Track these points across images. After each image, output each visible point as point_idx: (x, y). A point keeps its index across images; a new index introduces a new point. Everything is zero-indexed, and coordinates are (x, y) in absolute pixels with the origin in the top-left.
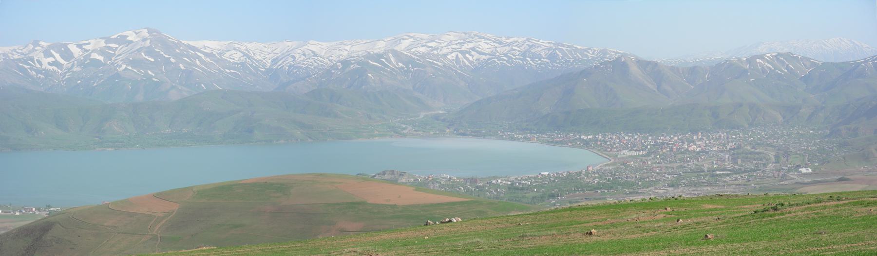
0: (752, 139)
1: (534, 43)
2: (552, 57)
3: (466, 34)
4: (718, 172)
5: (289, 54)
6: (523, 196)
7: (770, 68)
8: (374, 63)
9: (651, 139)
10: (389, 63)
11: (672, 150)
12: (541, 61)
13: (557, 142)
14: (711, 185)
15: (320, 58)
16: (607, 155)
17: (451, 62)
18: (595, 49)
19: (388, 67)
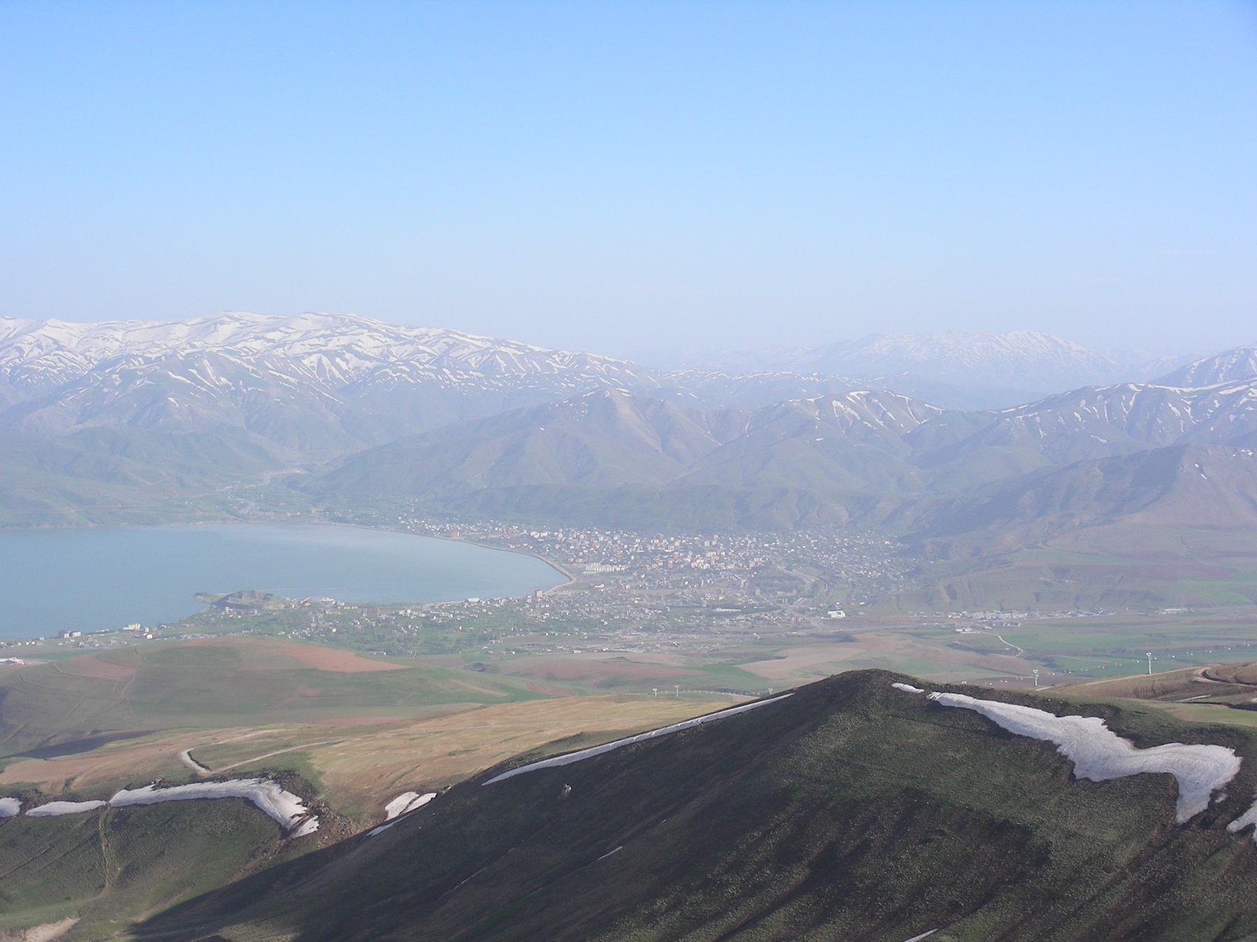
0: (793, 550)
1: (456, 339)
2: (488, 367)
3: (335, 318)
4: (718, 610)
5: (12, 344)
6: (444, 638)
7: (854, 418)
8: (178, 377)
9: (639, 544)
10: (204, 378)
11: (666, 563)
12: (468, 375)
13: (492, 541)
15: (69, 354)
16: (568, 570)
18: (565, 353)
19: (203, 384)
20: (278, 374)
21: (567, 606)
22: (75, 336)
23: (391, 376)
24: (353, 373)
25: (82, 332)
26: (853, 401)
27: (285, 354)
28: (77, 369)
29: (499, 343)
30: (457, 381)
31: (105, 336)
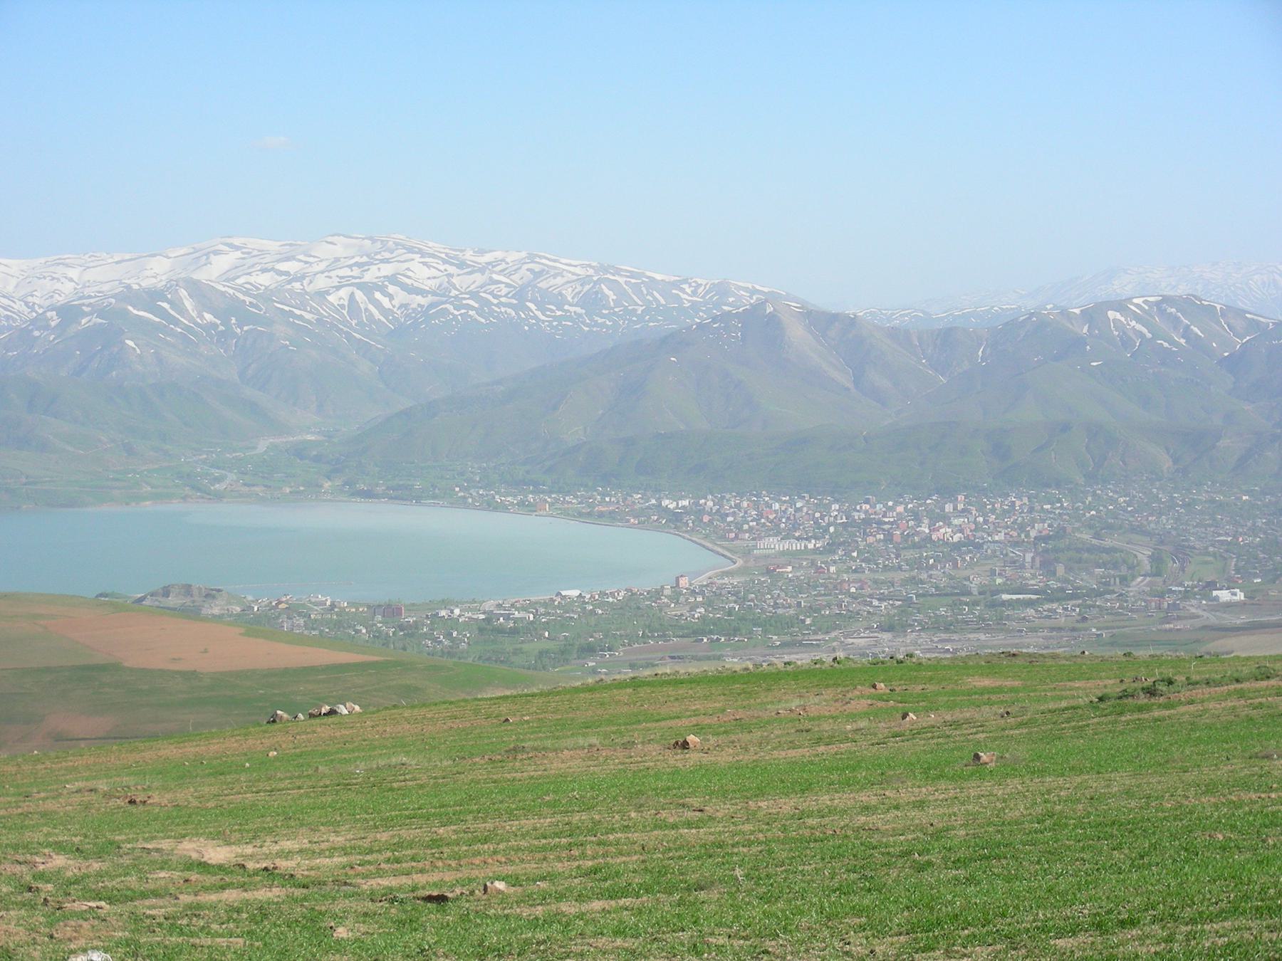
2: (592, 301)
3: (373, 240)
4: (1005, 597)
7: (1142, 335)
8: (141, 313)
13: (601, 515)
14: (987, 629)
16: (728, 550)
18: (700, 281)
19: (177, 322)
20: (287, 308)
21: (734, 598)
22: (13, 276)
23: (452, 314)
24: (399, 312)
25: (22, 271)
26: (1137, 311)
27: (303, 289)
28: (14, 320)
29: (605, 269)
30: (547, 319)
31: (54, 275)
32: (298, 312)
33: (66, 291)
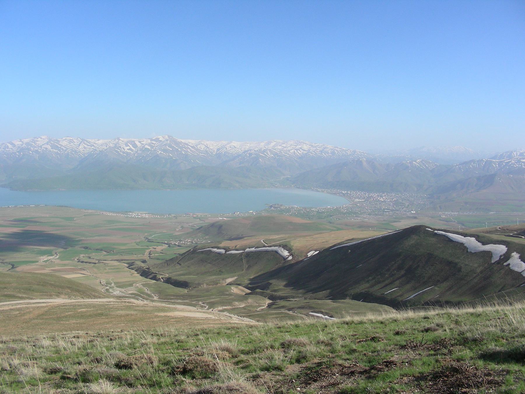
2: (333, 153)
3: (298, 141)
4: (386, 210)
11: (374, 199)
13: (333, 193)
14: (381, 215)
17: (292, 154)
32: (286, 155)
33: (247, 148)
